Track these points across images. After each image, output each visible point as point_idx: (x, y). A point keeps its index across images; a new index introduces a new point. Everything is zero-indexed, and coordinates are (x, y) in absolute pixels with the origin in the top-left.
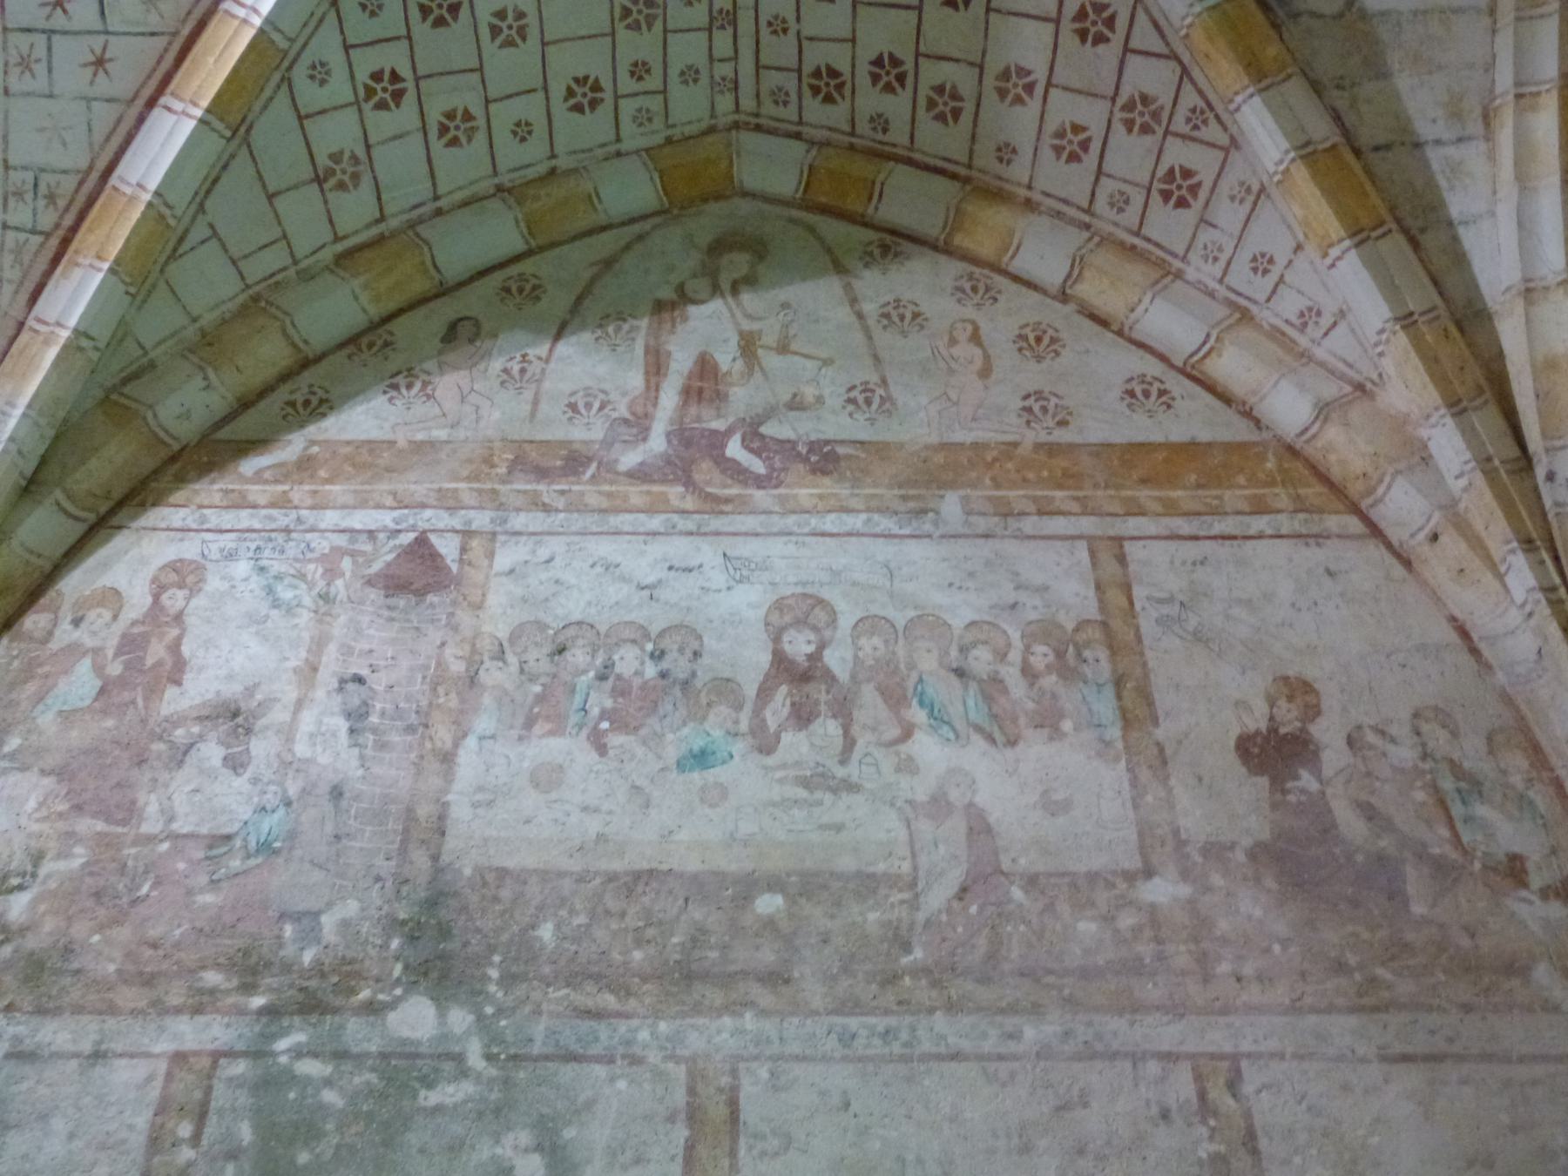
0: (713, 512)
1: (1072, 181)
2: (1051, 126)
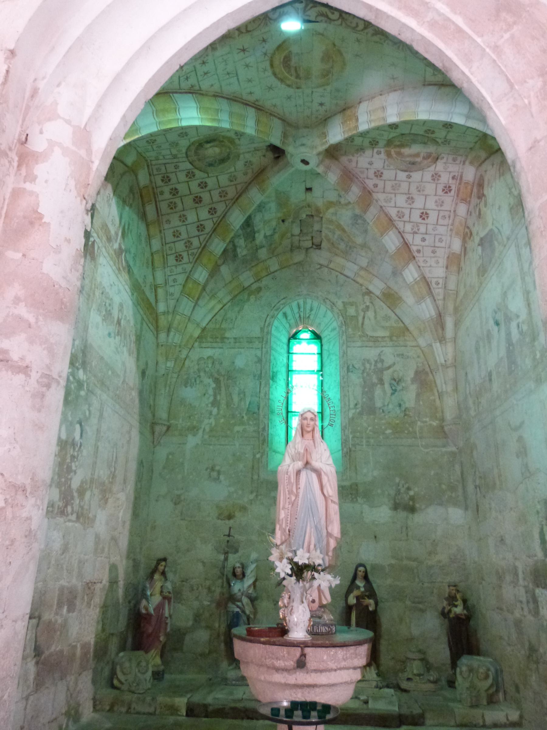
0: (270, 363)
1: (170, 238)
2: (178, 229)
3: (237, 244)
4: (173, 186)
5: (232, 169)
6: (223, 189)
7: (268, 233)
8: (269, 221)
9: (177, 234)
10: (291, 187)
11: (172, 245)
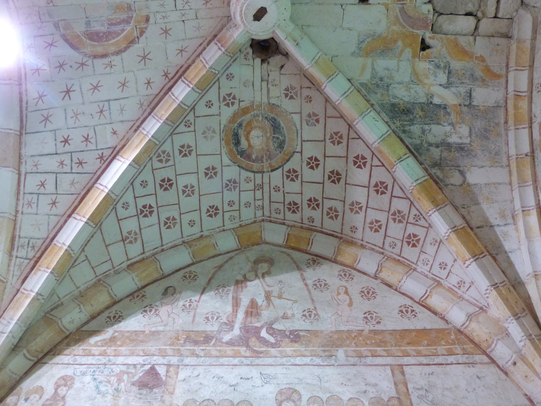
1: (377, 238)
3: (439, 140)
4: (305, 202)
5: (296, 118)
6: (328, 137)
7: (443, 78)
8: (415, 73)
9: (376, 227)
10: (350, 29)
11: (388, 240)
